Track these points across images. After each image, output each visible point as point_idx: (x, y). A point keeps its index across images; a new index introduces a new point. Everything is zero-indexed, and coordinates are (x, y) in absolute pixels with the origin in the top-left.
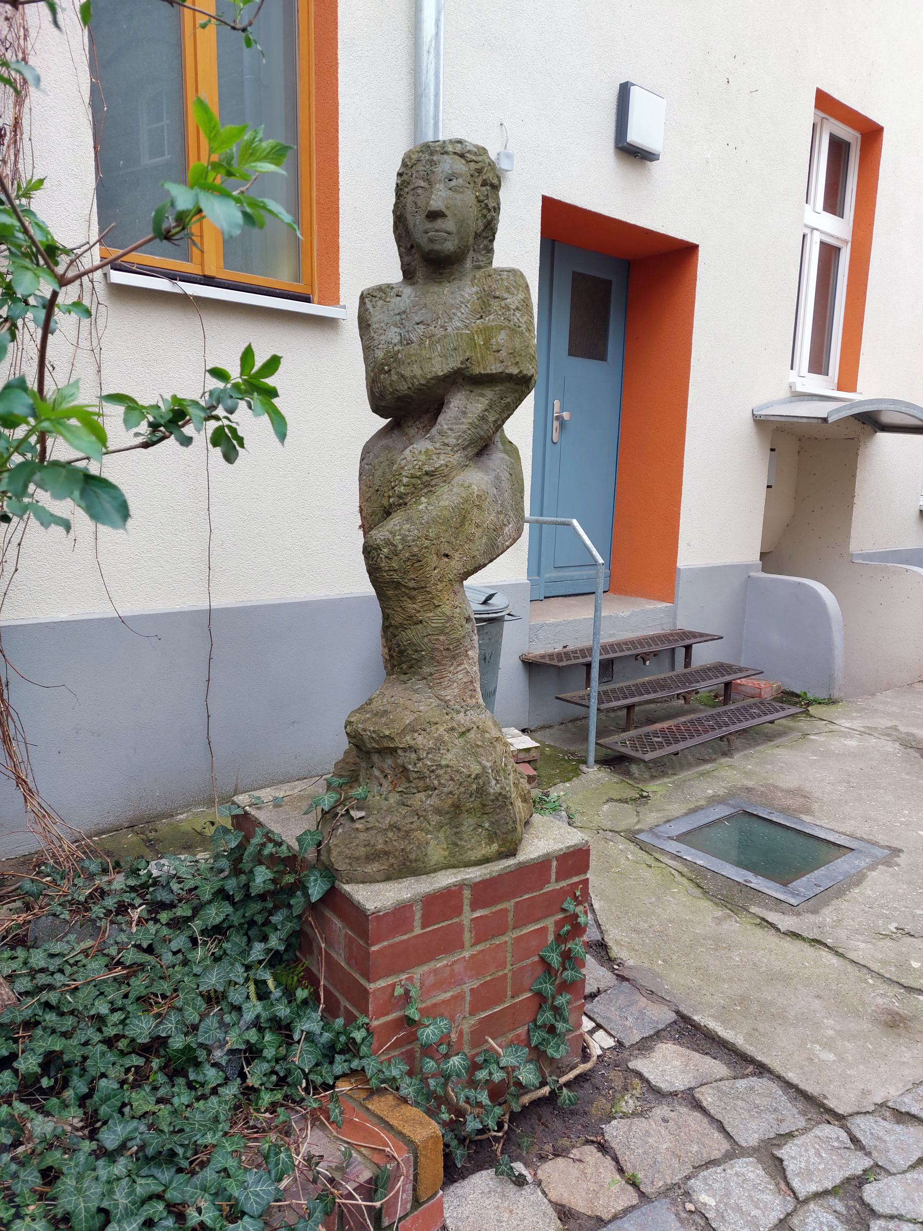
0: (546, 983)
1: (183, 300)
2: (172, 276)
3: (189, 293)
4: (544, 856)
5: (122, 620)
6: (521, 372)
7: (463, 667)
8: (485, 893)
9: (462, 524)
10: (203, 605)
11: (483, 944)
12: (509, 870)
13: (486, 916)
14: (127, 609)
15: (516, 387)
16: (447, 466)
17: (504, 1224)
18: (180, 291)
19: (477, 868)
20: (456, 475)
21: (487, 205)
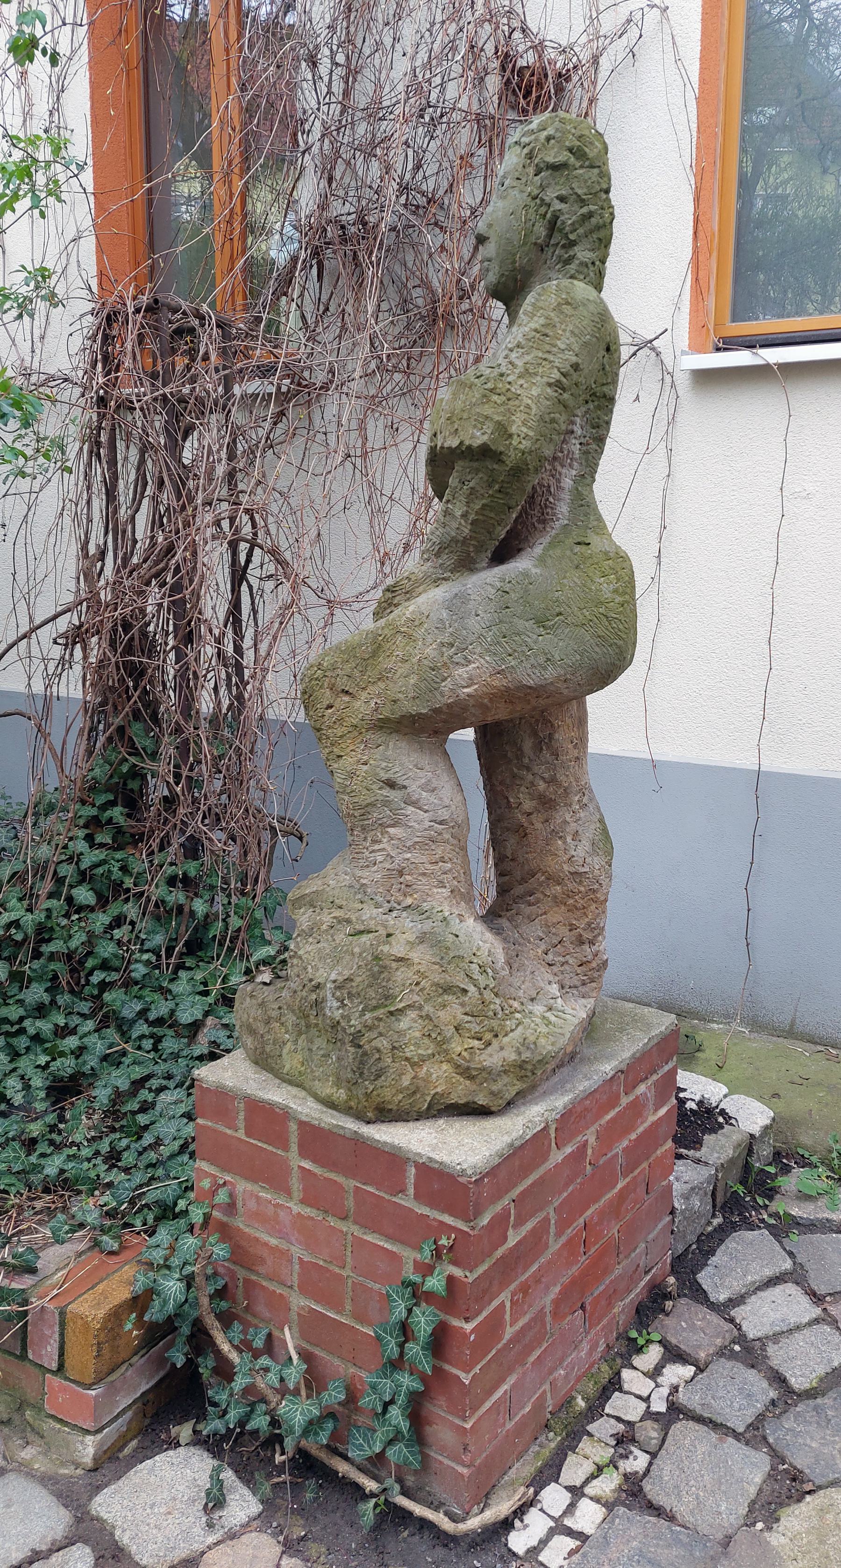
0: (392, 1336)
1: (762, 372)
2: (750, 344)
3: (772, 361)
4: (393, 1146)
5: (654, 764)
6: (461, 443)
7: (381, 846)
8: (315, 1140)
9: (374, 654)
10: (748, 762)
11: (315, 1211)
12: (342, 1132)
13: (315, 1175)
14: (665, 752)
15: (475, 464)
16: (410, 579)
17: (149, 1511)
18: (762, 362)
19: (319, 1107)
20: (425, 591)
21: (542, 200)
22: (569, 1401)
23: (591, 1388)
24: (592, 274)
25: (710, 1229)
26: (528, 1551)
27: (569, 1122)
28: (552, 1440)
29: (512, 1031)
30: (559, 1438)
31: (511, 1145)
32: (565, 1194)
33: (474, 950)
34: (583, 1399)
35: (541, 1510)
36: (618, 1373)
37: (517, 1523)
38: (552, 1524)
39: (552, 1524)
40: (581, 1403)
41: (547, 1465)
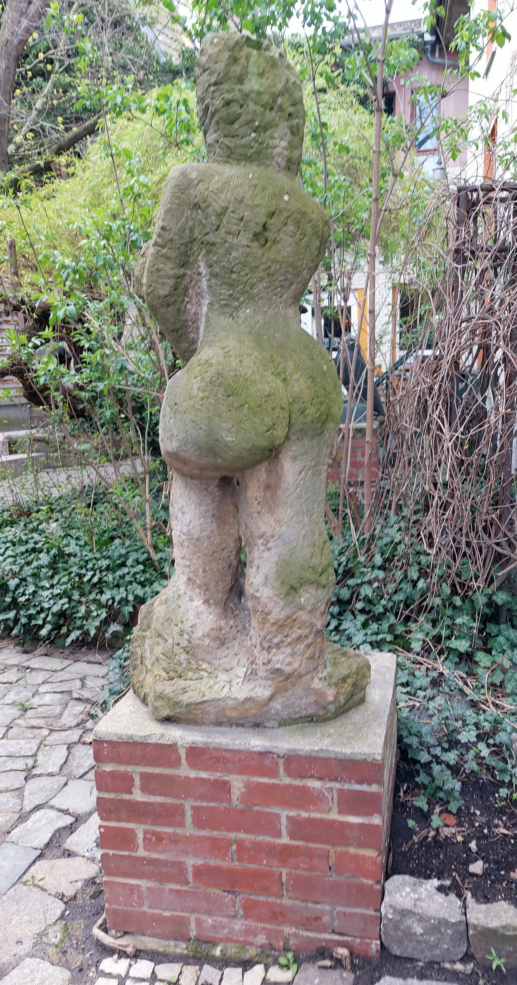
22: (213, 943)
23: (232, 951)
24: (218, 150)
25: (447, 965)
26: (102, 971)
27: (196, 754)
28: (181, 948)
29: (191, 679)
30: (185, 952)
31: (131, 737)
32: (204, 804)
33: (184, 619)
34: (221, 951)
35: (130, 965)
36: (258, 963)
37: (116, 956)
38: (123, 975)
39: (123, 975)
40: (217, 952)
41: (159, 954)
